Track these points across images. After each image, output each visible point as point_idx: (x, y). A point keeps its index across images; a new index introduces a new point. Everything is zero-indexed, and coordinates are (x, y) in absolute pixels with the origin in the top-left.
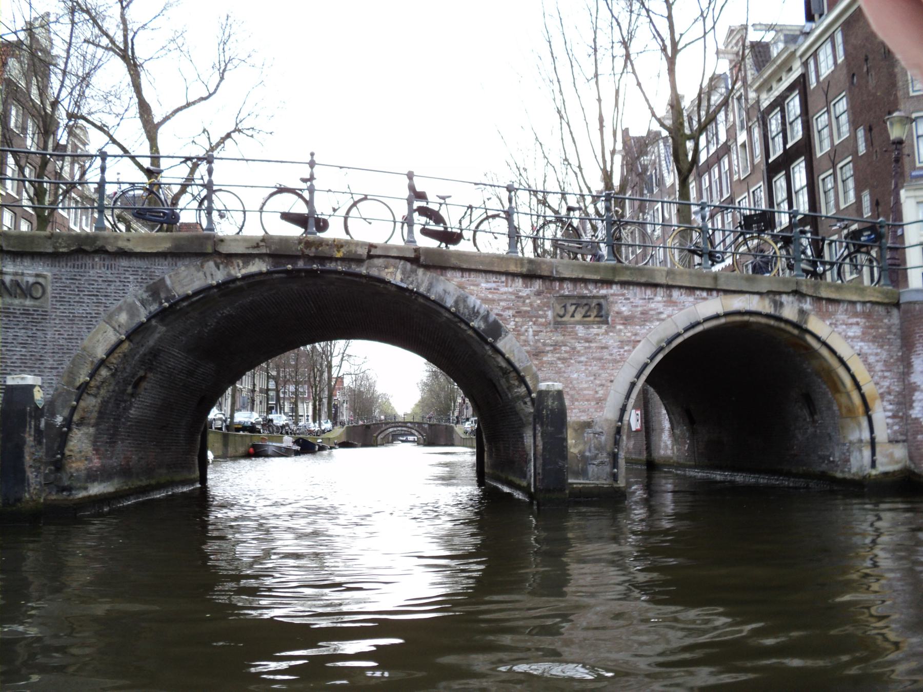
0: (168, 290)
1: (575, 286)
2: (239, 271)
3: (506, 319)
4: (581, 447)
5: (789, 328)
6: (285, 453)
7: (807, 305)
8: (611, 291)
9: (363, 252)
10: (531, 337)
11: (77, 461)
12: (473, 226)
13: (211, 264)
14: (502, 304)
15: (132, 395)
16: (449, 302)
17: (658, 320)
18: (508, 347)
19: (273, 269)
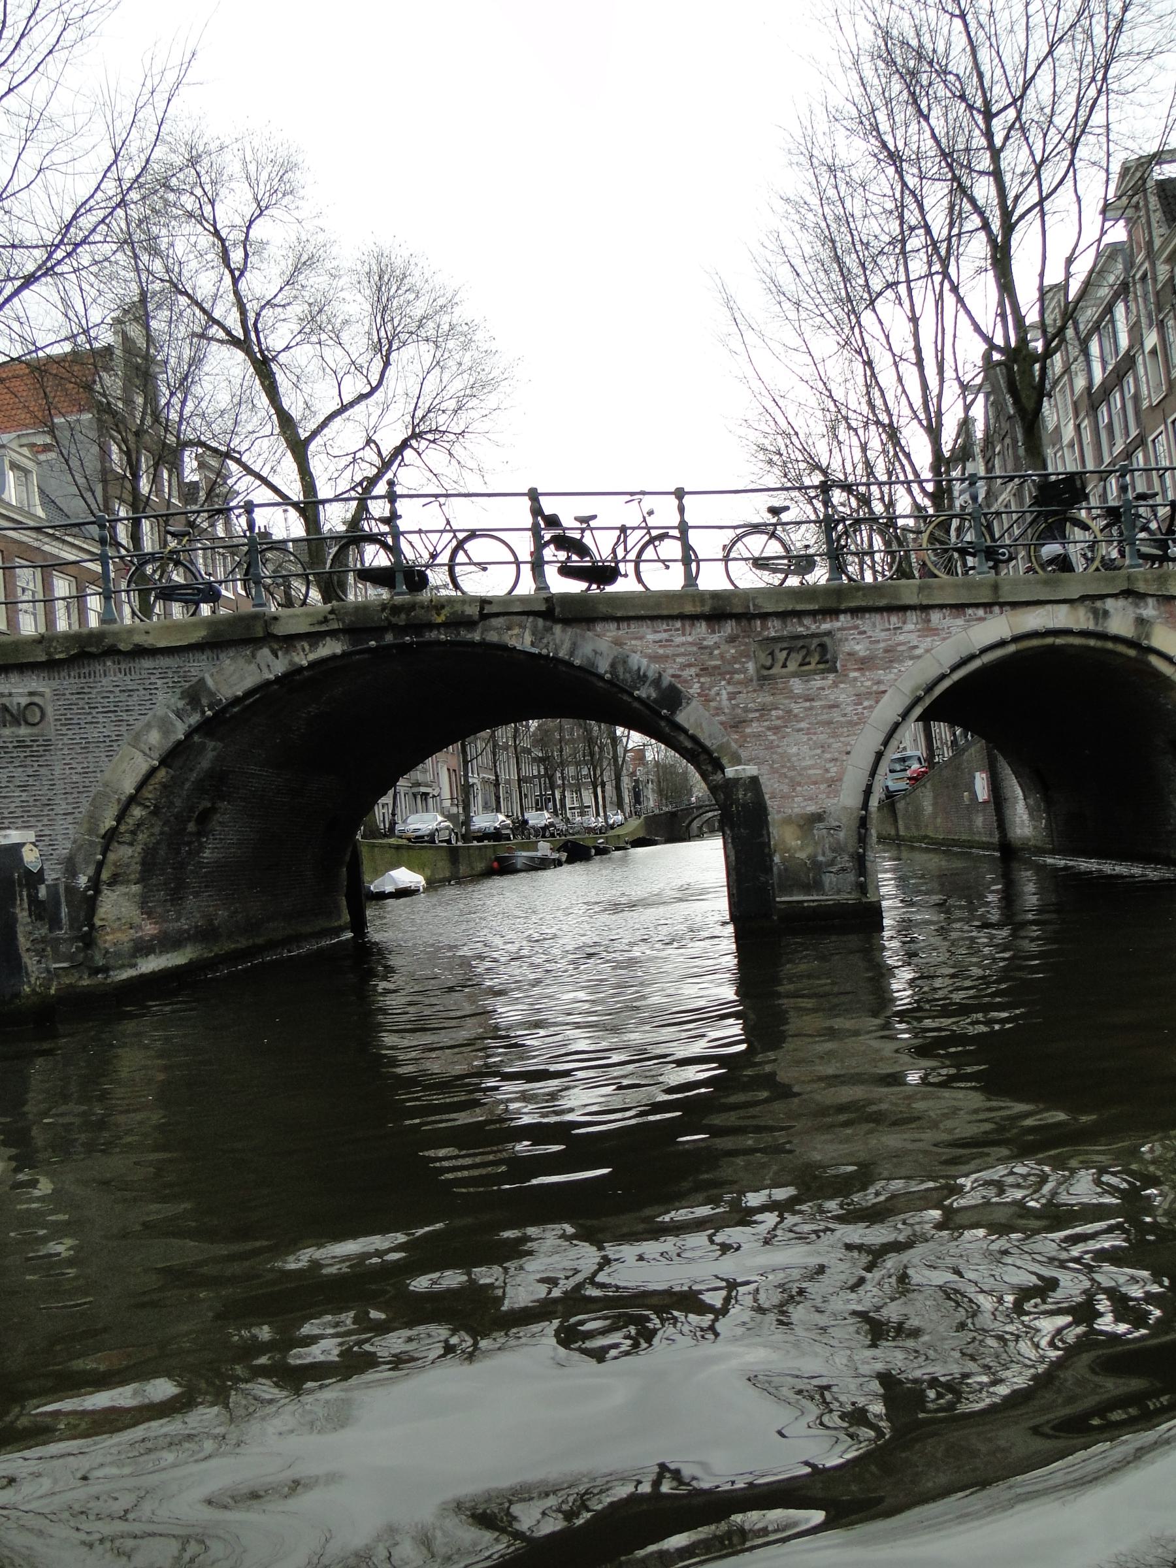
0: (212, 694)
1: (784, 623)
2: (304, 657)
3: (686, 681)
4: (810, 850)
5: (1121, 648)
6: (543, 864)
7: (1149, 610)
8: (838, 624)
9: (472, 611)
10: (725, 703)
11: (114, 931)
12: (632, 556)
13: (266, 651)
14: (679, 660)
15: (199, 834)
16: (603, 667)
17: (912, 658)
18: (692, 720)
19: (351, 649)
